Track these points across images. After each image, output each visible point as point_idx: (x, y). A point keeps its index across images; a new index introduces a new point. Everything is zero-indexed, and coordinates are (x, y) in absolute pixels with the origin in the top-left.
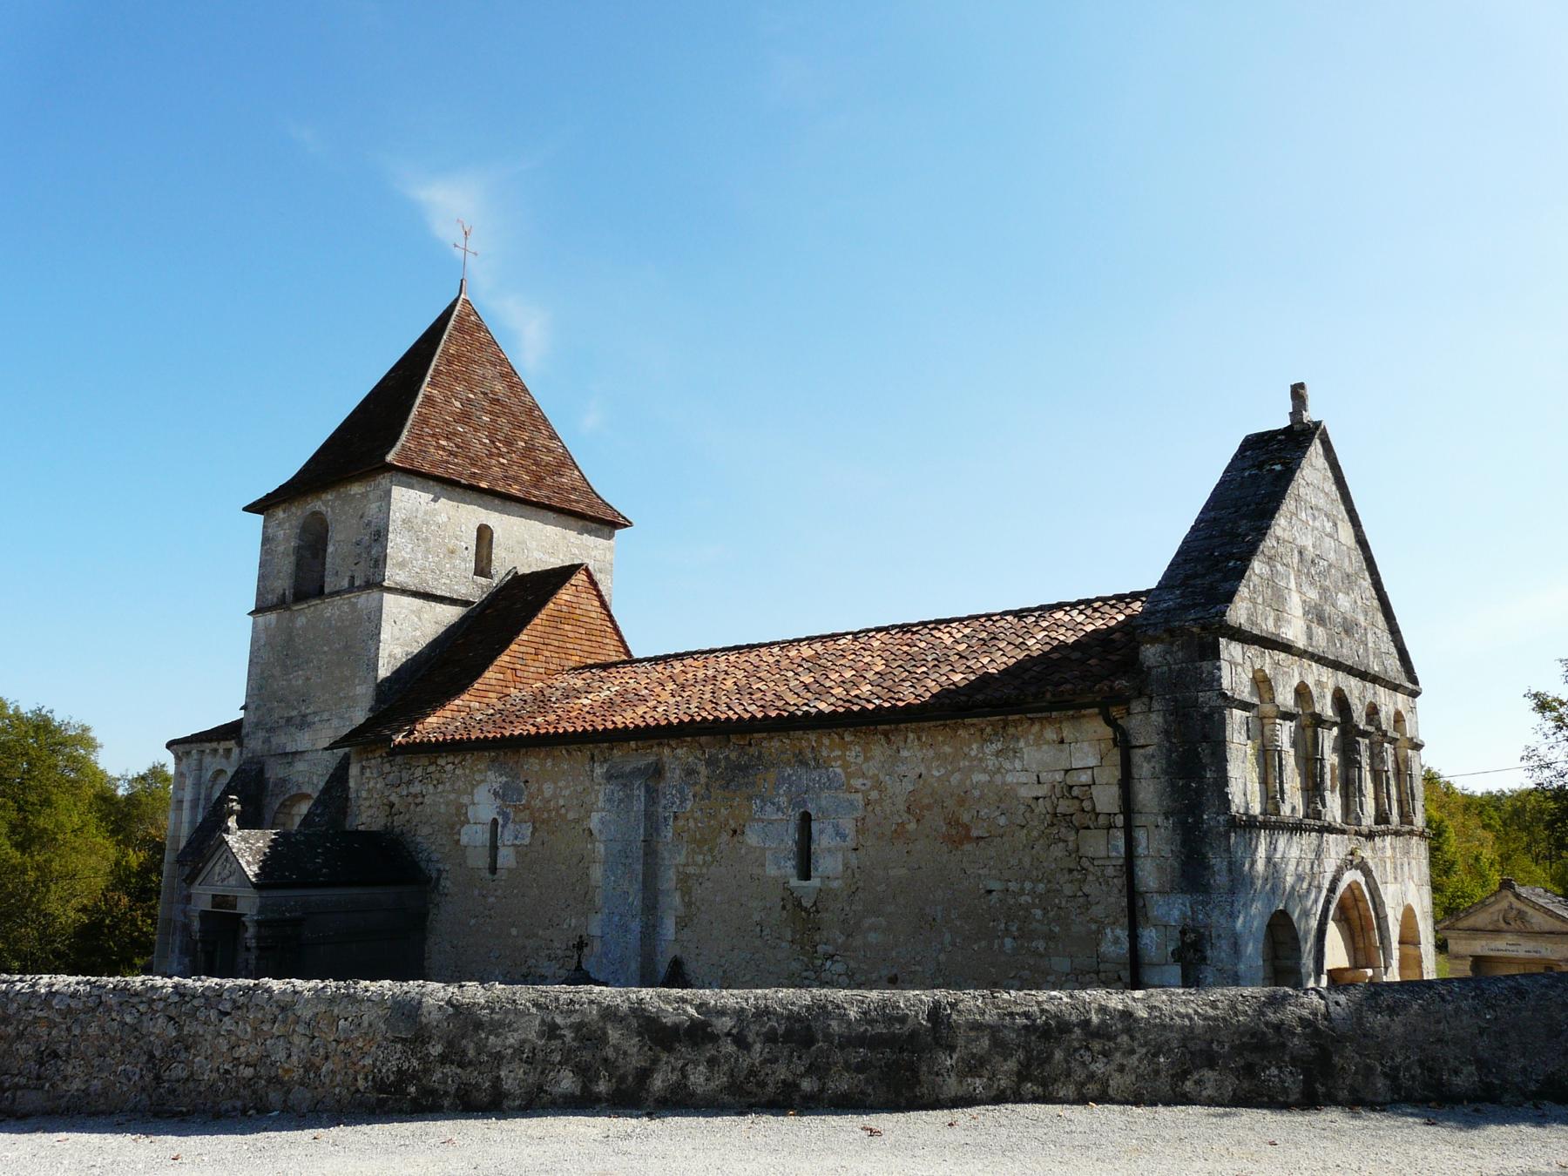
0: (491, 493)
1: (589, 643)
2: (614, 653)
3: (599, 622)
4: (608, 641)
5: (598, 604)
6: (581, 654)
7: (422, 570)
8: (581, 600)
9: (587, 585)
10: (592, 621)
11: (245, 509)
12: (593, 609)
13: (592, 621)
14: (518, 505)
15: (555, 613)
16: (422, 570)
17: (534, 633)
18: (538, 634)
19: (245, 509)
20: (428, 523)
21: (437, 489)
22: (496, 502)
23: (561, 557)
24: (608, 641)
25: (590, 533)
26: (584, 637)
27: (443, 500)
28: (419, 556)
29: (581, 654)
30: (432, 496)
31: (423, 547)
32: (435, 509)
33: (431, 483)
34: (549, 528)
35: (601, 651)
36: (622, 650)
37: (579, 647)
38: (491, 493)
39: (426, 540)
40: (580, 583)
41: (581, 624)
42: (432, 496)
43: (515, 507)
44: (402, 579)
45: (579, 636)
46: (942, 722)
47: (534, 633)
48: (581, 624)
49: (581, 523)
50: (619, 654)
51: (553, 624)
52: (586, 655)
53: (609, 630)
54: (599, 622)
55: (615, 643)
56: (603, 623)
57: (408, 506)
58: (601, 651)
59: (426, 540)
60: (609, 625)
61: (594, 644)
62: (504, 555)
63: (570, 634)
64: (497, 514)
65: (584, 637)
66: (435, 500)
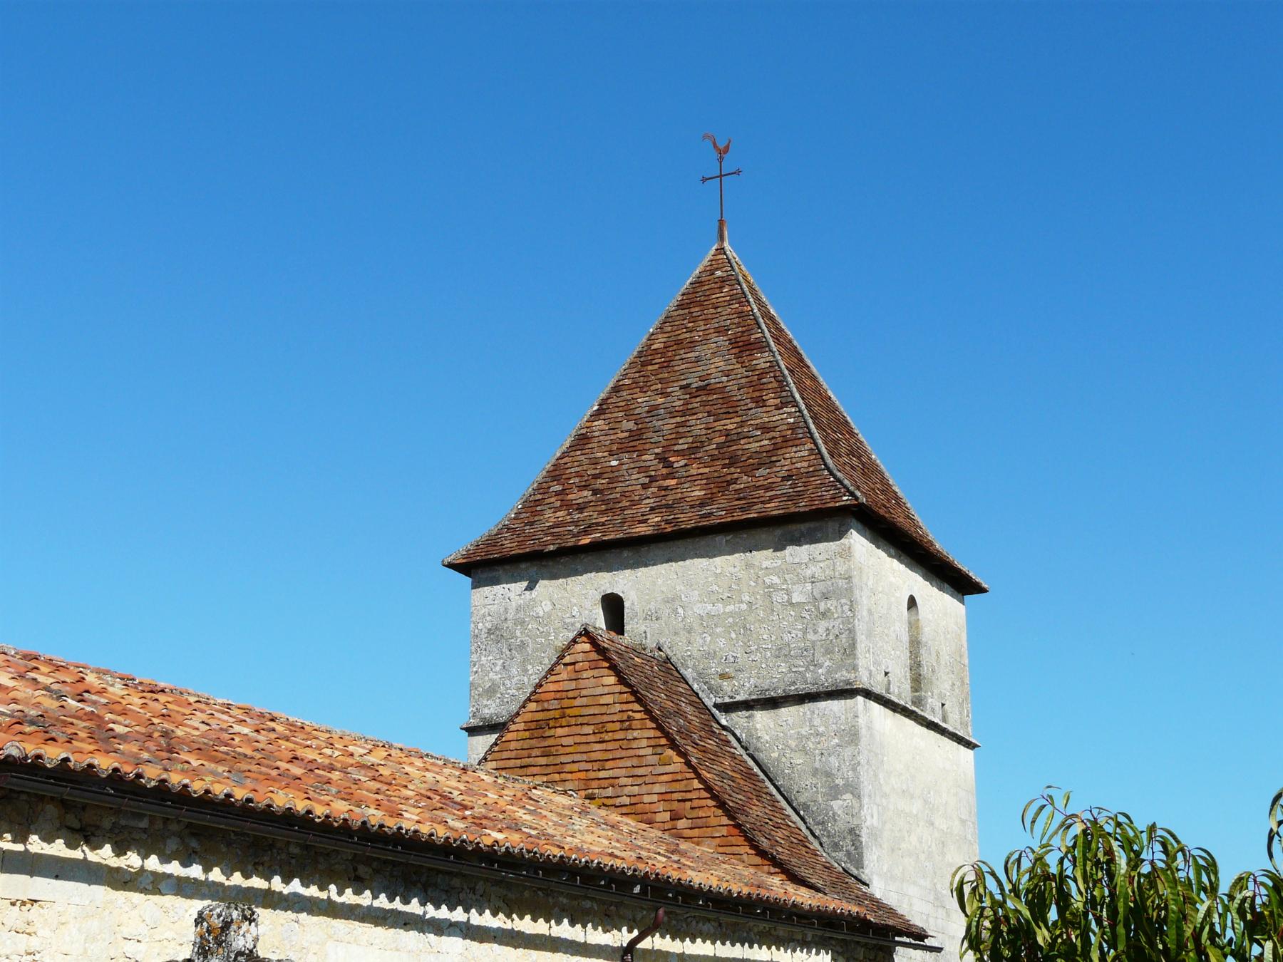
0: (598, 548)
1: (603, 746)
2: (650, 751)
3: (618, 707)
4: (636, 734)
5: (612, 680)
6: (589, 766)
7: (518, 689)
8: (583, 683)
9: (594, 656)
10: (603, 710)
11: (983, 590)
12: (606, 690)
13: (603, 710)
14: (662, 545)
15: (540, 716)
16: (518, 689)
17: (505, 755)
18: (513, 754)
19: (983, 590)
20: (523, 622)
21: (533, 570)
22: (625, 554)
23: (746, 598)
24: (636, 734)
25: (797, 542)
26: (592, 738)
27: (542, 583)
28: (514, 671)
29: (589, 766)
30: (525, 584)
31: (519, 657)
32: (533, 600)
33: (523, 566)
34: (718, 561)
35: (624, 753)
36: (663, 741)
37: (584, 757)
38: (598, 548)
39: (523, 645)
40: (580, 657)
41: (585, 720)
42: (525, 584)
43: (656, 550)
44: (492, 711)
45: (583, 739)
46: (129, 869)
47: (505, 755)
48: (585, 720)
49: (778, 532)
50: (659, 750)
51: (537, 733)
52: (596, 766)
53: (638, 716)
54: (618, 707)
55: (651, 733)
56: (625, 707)
57: (493, 608)
58: (624, 753)
59: (523, 645)
60: (637, 707)
61: (610, 746)
62: (643, 628)
63: (565, 741)
64: (628, 572)
65: (592, 738)
66: (530, 588)
